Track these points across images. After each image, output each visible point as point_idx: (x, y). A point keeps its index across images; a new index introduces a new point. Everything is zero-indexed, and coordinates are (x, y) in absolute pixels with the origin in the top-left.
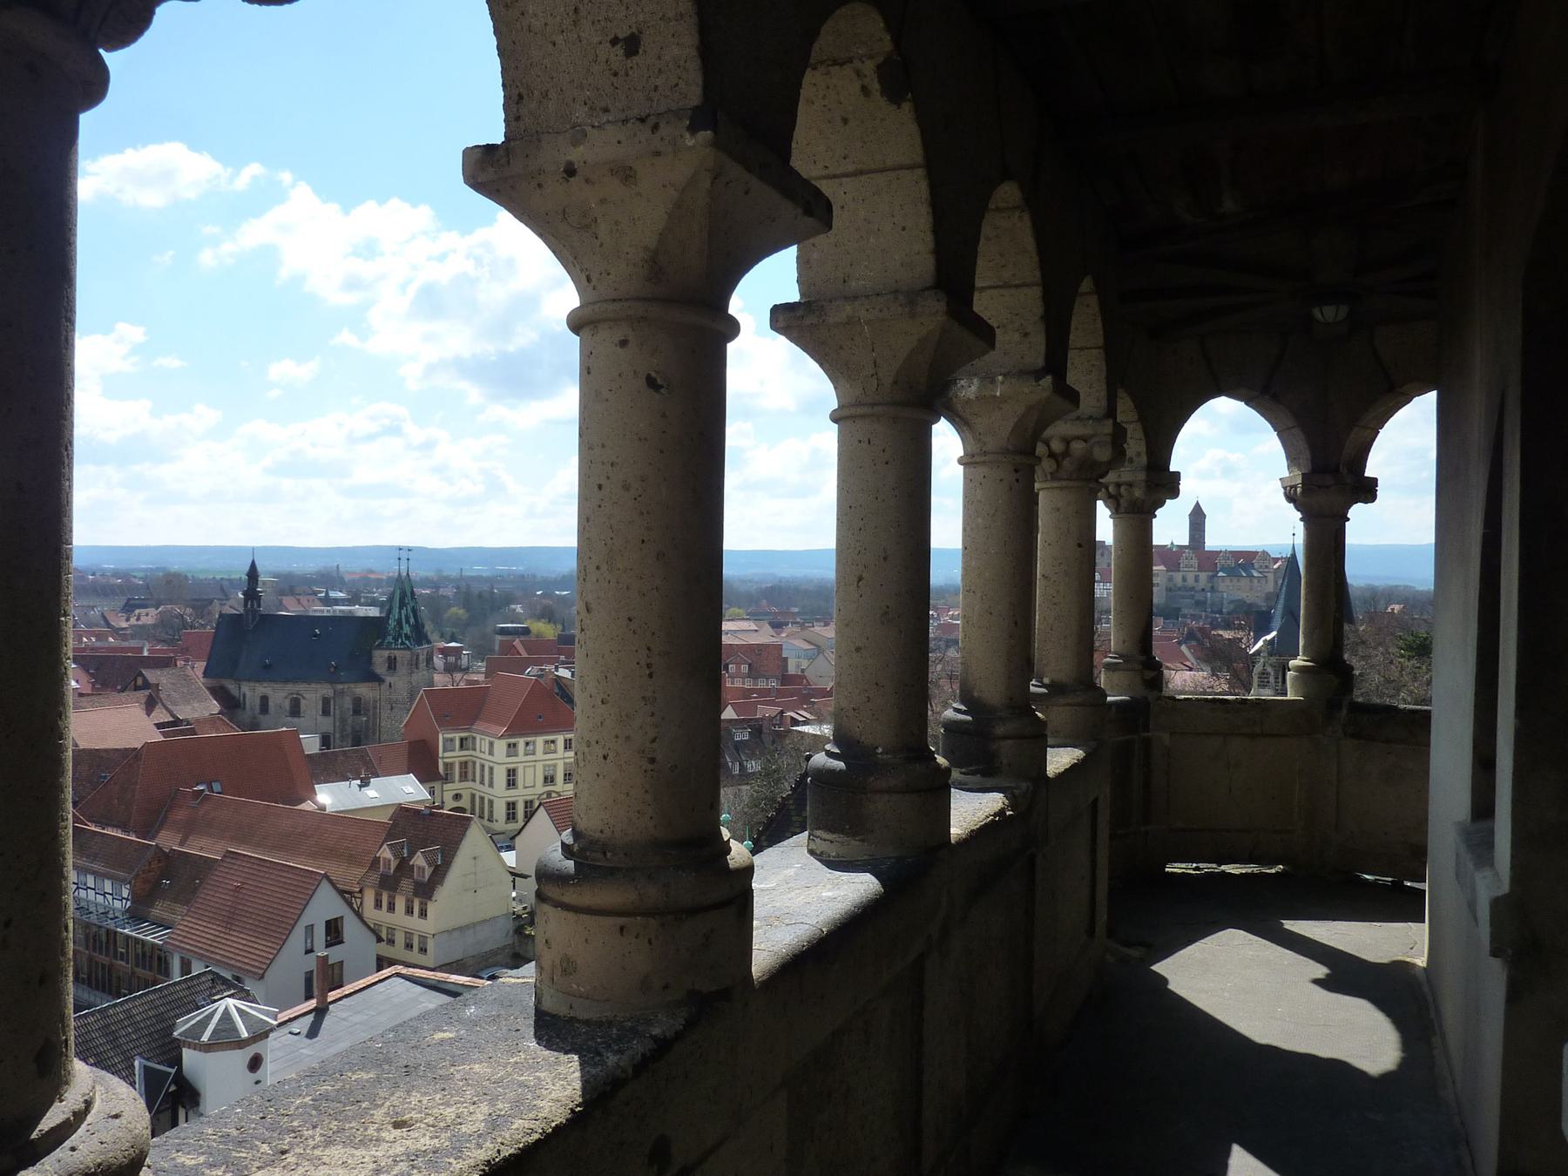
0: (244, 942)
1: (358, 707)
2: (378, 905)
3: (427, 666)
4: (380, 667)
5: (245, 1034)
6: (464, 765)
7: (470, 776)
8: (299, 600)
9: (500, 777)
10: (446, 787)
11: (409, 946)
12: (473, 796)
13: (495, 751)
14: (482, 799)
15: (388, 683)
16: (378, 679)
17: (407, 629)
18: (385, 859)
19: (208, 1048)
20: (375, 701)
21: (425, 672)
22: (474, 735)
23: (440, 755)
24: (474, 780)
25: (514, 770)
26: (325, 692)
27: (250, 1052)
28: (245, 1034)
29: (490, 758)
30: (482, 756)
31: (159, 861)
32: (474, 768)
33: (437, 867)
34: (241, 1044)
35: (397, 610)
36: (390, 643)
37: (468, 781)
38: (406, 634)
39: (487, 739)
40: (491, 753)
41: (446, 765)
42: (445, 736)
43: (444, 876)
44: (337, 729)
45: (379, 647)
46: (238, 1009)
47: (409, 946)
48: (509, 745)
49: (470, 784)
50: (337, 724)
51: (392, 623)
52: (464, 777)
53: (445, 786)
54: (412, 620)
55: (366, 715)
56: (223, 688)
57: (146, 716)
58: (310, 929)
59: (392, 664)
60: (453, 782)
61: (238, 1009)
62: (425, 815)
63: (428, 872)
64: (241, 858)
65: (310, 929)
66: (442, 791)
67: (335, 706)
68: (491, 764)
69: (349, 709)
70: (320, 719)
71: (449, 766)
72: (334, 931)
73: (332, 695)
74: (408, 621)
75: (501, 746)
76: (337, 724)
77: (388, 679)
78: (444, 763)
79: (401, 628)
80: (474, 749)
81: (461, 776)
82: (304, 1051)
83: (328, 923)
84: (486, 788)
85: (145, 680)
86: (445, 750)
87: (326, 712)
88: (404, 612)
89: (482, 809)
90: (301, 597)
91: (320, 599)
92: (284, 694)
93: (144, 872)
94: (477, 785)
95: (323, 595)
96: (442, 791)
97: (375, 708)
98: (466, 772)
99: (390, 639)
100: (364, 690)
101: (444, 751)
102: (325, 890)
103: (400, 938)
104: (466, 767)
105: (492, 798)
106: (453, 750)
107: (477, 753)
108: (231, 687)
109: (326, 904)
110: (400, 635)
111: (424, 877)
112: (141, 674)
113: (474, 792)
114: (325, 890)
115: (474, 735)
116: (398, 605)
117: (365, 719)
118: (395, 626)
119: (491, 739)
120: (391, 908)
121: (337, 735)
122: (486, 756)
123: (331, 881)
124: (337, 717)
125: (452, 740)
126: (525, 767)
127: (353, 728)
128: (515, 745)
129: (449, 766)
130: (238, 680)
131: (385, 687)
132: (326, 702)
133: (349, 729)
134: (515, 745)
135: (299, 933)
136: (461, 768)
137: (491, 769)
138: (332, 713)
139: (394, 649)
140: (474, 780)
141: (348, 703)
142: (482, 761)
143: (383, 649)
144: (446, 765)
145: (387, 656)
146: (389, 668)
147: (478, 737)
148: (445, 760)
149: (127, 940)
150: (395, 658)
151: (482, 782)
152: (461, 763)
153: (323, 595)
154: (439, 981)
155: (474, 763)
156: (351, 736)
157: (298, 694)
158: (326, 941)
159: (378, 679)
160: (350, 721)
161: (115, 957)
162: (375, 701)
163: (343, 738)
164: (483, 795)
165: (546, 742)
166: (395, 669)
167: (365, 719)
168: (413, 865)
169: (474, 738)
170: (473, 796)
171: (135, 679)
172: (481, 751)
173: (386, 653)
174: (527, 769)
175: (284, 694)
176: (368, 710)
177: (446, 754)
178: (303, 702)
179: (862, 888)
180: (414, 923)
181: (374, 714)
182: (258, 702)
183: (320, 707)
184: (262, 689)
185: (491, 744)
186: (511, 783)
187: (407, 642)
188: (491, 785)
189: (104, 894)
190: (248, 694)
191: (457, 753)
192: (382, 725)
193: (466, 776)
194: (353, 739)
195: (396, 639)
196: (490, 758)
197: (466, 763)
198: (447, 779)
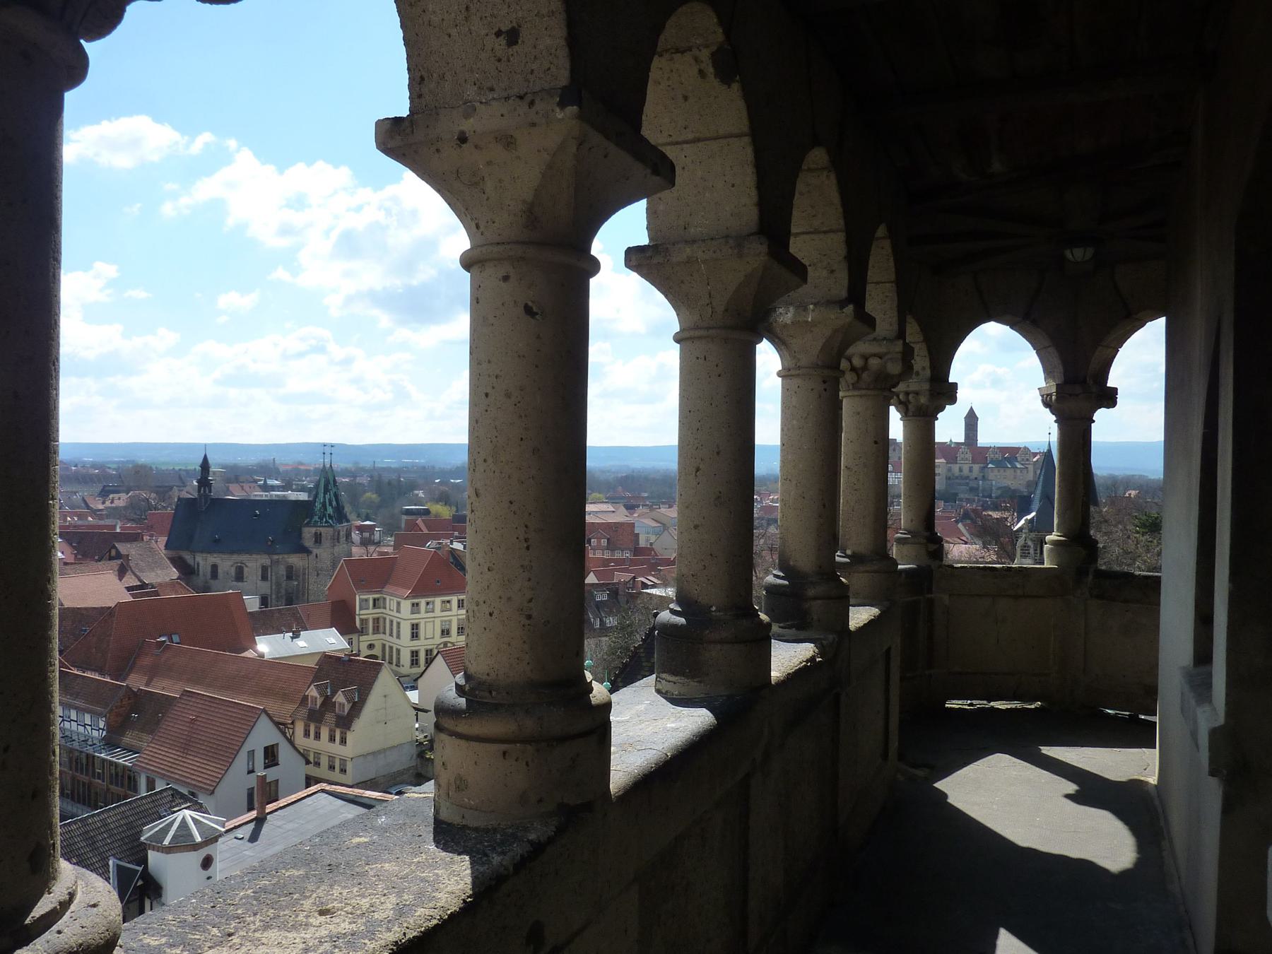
0: (198, 764)
1: (291, 573)
2: (307, 734)
3: (346, 540)
4: (308, 541)
5: (199, 839)
6: (376, 620)
7: (381, 629)
8: (242, 487)
9: (406, 630)
10: (362, 638)
11: (332, 768)
12: (384, 646)
13: (402, 610)
14: (391, 648)
15: (314, 554)
16: (307, 551)
17: (330, 510)
18: (312, 697)
19: (168, 850)
20: (304, 569)
21: (345, 545)
23: (357, 613)
24: (384, 633)
25: (417, 625)
26: (263, 561)
27: (202, 853)
28: (199, 839)
29: (397, 615)
30: (391, 613)
31: (129, 699)
32: (385, 623)
33: (355, 703)
34: (196, 847)
35: (322, 495)
36: (316, 522)
37: (379, 633)
38: (329, 515)
39: (395, 599)
40: (398, 611)
41: (362, 620)
42: (361, 597)
43: (360, 710)
44: (274, 592)
45: (308, 525)
46: (193, 819)
47: (332, 768)
48: (413, 605)
49: (381, 636)
50: (274, 587)
51: (318, 505)
52: (376, 630)
53: (361, 637)
54: (334, 503)
55: (297, 580)
56: (181, 558)
57: (118, 581)
58: (251, 754)
59: (318, 539)
60: (368, 634)
61: (193, 819)
62: (345, 661)
63: (347, 707)
64: (196, 696)
65: (251, 754)
66: (359, 642)
67: (271, 572)
68: (399, 620)
69: (283, 575)
70: (260, 583)
71: (364, 622)
72: (271, 756)
73: (270, 564)
74: (331, 504)
75: (406, 605)
76: (274, 587)
77: (315, 551)
78: (360, 619)
79: (326, 509)
80: (385, 608)
81: (374, 630)
82: (246, 853)
83: (266, 749)
84: (394, 640)
85: (118, 552)
86: (361, 609)
87: (264, 578)
88: (327, 496)
89: (391, 656)
90: (244, 485)
92: (230, 563)
93: (116, 707)
94: (387, 637)
95: (262, 482)
96: (359, 642)
97: (304, 574)
98: (378, 627)
99: (316, 518)
100: (295, 560)
101: (361, 609)
102: (264, 722)
103: (324, 761)
104: (378, 623)
105: (399, 647)
106: (368, 609)
107: (387, 611)
108: (188, 557)
109: (264, 734)
110: (325, 515)
111: (344, 711)
112: (114, 547)
113: (385, 642)
114: (264, 722)
115: (385, 596)
116: (323, 491)
117: (296, 583)
118: (320, 508)
119: (399, 600)
120: (317, 736)
121: (274, 597)
122: (395, 613)
123: (268, 715)
124: (274, 581)
125: (366, 600)
126: (426, 622)
127: (286, 590)
128: (417, 604)
129: (364, 622)
130: (193, 552)
131: (312, 557)
132: (264, 569)
133: (283, 591)
134: (417, 604)
135: (243, 757)
136: (374, 623)
137: (399, 624)
138: (269, 579)
139: (320, 527)
140: (384, 633)
141: (282, 570)
142: (391, 618)
143: (311, 526)
144: (362, 620)
145: (314, 532)
146: (316, 542)
147: (388, 598)
148: (361, 617)
149: (103, 762)
150: (321, 534)
151: (391, 635)
152: (374, 619)
153: (262, 482)
154: (356, 796)
155: (385, 619)
156: (284, 597)
157: (241, 563)
158: (265, 763)
159: (307, 551)
160: (284, 585)
161: (94, 776)
162: (304, 569)
163: (278, 598)
164: (392, 645)
165: (443, 602)
166: (320, 543)
167: (296, 583)
168: (335, 702)
169: (385, 599)
170: (384, 646)
171: (110, 551)
172: (390, 609)
173: (313, 530)
174: (428, 624)
175: (231, 563)
176: (299, 576)
177: (362, 612)
178: (246, 570)
179: (699, 720)
180: (336, 749)
181: (304, 579)
182: (209, 569)
183: (260, 573)
184: (213, 559)
185: (399, 604)
186: (415, 635)
187: (330, 521)
188: (398, 637)
189: (84, 726)
190: (201, 563)
191: (371, 611)
192: (310, 588)
193: (378, 630)
194: (286, 600)
195: (321, 519)
196: (397, 615)
197: (378, 619)
198: (362, 632)
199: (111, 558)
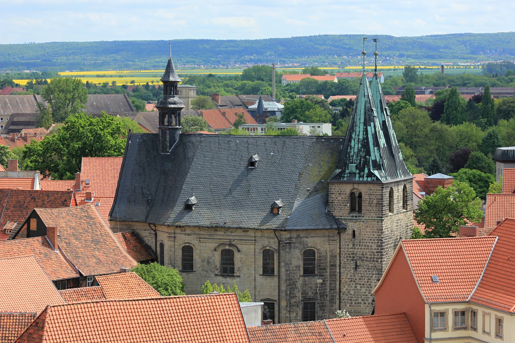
3: (404, 207)
8: (224, 114)
17: (375, 154)
20: (333, 257)
21: (401, 216)
22: (474, 307)
23: (427, 335)
26: (266, 242)
35: (362, 126)
36: (352, 174)
38: (375, 162)
42: (433, 308)
44: (283, 295)
51: (355, 145)
54: (382, 141)
56: (135, 235)
70: (261, 280)
73: (275, 246)
74: (377, 144)
76: (283, 288)
77: (351, 226)
79: (368, 153)
80: (475, 329)
85: (40, 222)
86: (432, 330)
91: (252, 112)
97: (333, 266)
99: (352, 167)
101: (432, 330)
106: (445, 329)
110: (366, 163)
112: (34, 214)
115: (474, 307)
116: (362, 121)
117: (320, 281)
118: (359, 151)
119: (500, 315)
121: (283, 303)
124: (283, 277)
125: (442, 314)
127: (304, 293)
131: (346, 236)
132: (267, 255)
133: (299, 296)
138: (276, 273)
139: (359, 183)
145: (348, 191)
146: (352, 209)
147: (480, 311)
150: (360, 196)
153: (255, 106)
157: (230, 245)
160: (299, 283)
166: (360, 211)
167: (320, 281)
169: (474, 313)
171: (28, 222)
172: (484, 331)
173: (347, 189)
175: (214, 245)
177: (435, 335)
178: (237, 256)
183: (260, 262)
185: (499, 322)
187: (376, 173)
190: (167, 244)
192: (344, 290)
195: (360, 168)
199: (30, 234)
